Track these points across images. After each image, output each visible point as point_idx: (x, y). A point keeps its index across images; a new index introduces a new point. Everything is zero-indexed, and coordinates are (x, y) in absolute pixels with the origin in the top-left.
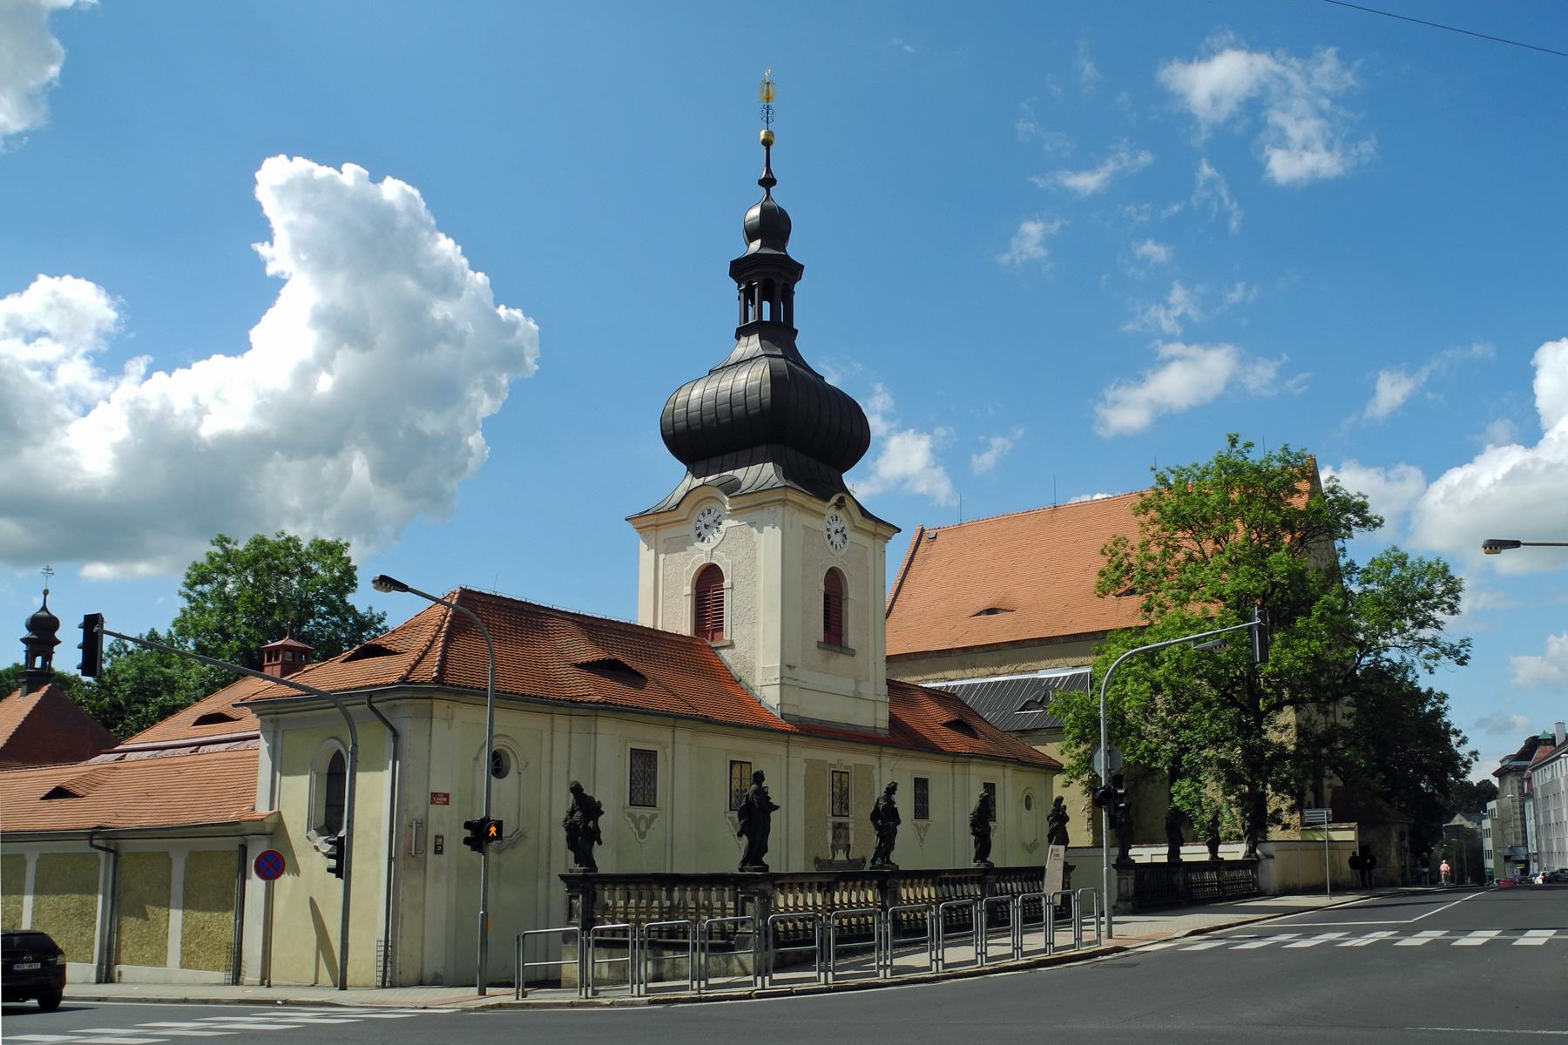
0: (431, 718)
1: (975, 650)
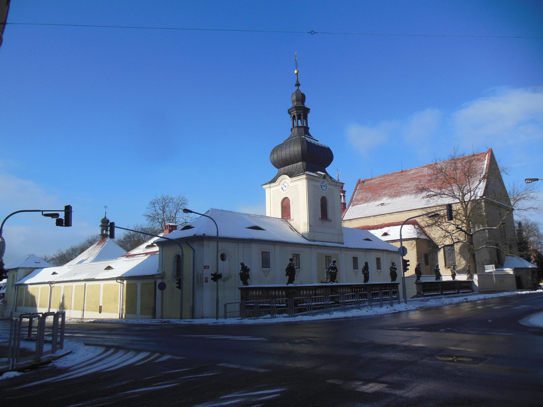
0: (203, 245)
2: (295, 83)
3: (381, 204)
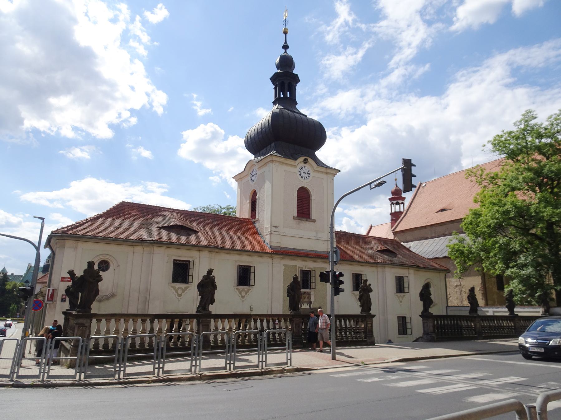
1: (436, 225)
2: (283, 44)
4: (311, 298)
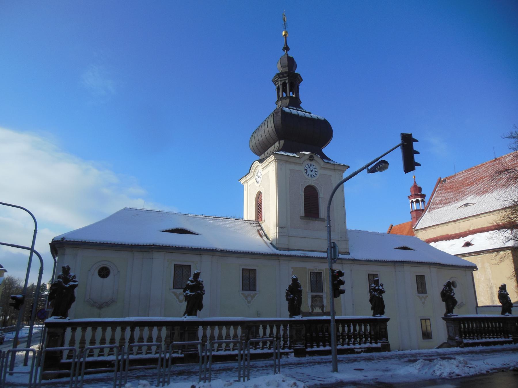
2: (283, 45)
3: (464, 205)
4: (323, 302)
